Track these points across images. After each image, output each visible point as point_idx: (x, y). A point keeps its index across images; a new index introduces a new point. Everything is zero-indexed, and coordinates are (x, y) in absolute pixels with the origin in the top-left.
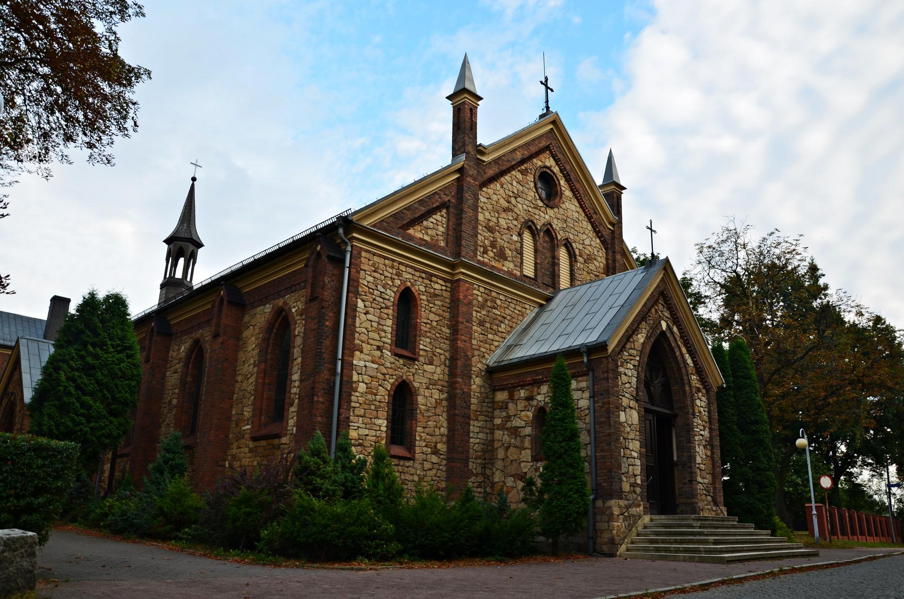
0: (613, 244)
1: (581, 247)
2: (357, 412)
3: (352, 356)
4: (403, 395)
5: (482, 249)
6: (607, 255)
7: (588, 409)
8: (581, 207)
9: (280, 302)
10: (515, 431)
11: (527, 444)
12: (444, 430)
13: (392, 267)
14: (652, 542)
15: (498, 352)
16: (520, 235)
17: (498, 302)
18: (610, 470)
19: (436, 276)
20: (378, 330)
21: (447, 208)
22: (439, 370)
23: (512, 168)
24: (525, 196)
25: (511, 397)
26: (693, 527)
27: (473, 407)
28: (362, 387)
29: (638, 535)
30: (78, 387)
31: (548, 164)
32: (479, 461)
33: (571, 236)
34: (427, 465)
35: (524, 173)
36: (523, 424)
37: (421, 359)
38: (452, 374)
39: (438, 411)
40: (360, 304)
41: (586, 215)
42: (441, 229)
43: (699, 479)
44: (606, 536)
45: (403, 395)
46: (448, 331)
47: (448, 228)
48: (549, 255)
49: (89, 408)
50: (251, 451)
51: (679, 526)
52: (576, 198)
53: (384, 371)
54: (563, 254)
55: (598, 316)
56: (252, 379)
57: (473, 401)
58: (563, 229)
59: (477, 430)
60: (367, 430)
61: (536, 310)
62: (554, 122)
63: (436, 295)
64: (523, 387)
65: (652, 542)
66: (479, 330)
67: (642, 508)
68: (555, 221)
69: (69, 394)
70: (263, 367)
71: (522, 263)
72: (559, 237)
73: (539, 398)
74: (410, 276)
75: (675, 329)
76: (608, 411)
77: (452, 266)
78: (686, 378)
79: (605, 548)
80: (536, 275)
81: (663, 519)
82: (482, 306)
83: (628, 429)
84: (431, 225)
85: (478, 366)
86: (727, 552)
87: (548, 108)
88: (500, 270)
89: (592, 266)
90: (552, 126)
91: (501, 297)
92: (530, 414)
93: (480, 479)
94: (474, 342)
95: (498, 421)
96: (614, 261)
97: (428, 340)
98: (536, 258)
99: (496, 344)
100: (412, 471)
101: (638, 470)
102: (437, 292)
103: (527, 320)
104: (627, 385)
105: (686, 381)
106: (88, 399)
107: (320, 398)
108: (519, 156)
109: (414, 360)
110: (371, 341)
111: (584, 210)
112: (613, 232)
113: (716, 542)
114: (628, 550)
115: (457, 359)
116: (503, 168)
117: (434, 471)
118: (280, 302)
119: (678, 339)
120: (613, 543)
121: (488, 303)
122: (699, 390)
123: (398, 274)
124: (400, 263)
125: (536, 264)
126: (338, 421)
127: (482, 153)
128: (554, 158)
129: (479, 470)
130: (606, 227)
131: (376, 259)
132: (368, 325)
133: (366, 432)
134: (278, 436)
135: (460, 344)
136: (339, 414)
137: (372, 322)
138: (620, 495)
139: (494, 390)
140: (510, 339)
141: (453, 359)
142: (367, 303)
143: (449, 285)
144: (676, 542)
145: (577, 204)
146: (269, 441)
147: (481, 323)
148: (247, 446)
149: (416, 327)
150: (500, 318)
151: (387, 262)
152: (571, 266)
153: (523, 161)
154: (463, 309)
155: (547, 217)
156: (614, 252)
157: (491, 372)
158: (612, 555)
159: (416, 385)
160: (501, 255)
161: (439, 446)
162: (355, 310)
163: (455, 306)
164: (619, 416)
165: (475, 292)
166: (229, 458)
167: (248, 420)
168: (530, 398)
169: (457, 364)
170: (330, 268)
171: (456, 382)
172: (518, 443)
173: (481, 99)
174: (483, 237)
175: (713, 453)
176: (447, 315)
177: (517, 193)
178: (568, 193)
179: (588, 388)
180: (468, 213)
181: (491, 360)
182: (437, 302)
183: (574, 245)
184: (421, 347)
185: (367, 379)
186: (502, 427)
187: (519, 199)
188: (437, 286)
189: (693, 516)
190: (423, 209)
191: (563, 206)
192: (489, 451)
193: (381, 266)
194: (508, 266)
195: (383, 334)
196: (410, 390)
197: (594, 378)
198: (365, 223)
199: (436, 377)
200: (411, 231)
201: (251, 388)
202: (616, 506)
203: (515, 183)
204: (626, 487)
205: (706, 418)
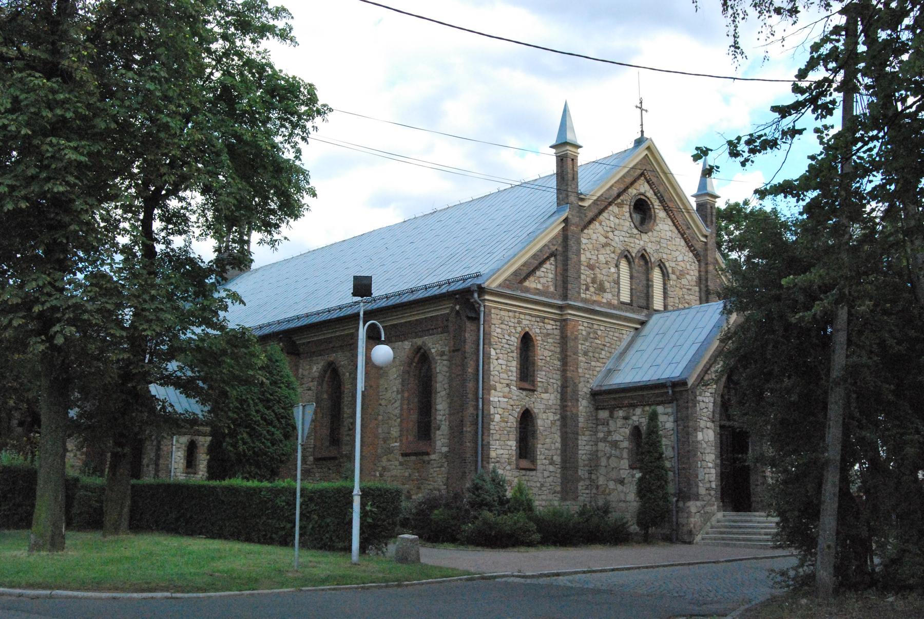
1: (673, 264)
2: (494, 438)
3: (489, 394)
4: (526, 418)
5: (584, 287)
9: (419, 341)
10: (615, 445)
11: (625, 455)
12: (558, 445)
13: (515, 317)
14: (721, 533)
15: (600, 376)
16: (617, 266)
17: (599, 333)
19: (548, 318)
20: (506, 371)
21: (555, 256)
23: (610, 204)
24: (621, 228)
25: (611, 416)
27: (580, 425)
28: (497, 418)
29: (712, 528)
31: (642, 191)
32: (587, 468)
33: (665, 256)
34: (546, 474)
35: (620, 205)
36: (622, 438)
37: (539, 389)
38: (563, 398)
39: (553, 430)
40: (493, 352)
41: (679, 232)
44: (685, 529)
45: (526, 418)
46: (559, 363)
47: (556, 275)
48: (643, 278)
50: (401, 464)
52: (670, 217)
53: (512, 403)
54: (656, 275)
55: (682, 352)
56: (397, 404)
57: (581, 419)
58: (657, 251)
59: (584, 443)
60: (502, 448)
61: (632, 334)
62: (648, 148)
63: (548, 335)
64: (621, 408)
65: (721, 533)
66: (584, 359)
67: (715, 507)
68: (649, 245)
70: (406, 395)
71: (619, 292)
72: (653, 260)
73: (635, 418)
74: (528, 322)
76: (688, 434)
77: (560, 308)
79: (686, 537)
81: (732, 515)
82: (586, 340)
83: (705, 445)
84: (542, 274)
85: (584, 390)
87: (642, 132)
88: (599, 303)
89: (684, 281)
90: (646, 152)
91: (602, 328)
92: (627, 431)
93: (588, 483)
94: (580, 370)
95: (601, 435)
96: (707, 272)
97: (544, 373)
98: (631, 284)
99: (598, 369)
100: (536, 479)
101: (713, 477)
102: (549, 332)
103: (624, 344)
104: (705, 410)
107: (468, 428)
108: (615, 191)
109: (534, 391)
110: (502, 381)
111: (677, 228)
112: (706, 243)
114: (703, 539)
115: (567, 387)
116: (604, 205)
117: (551, 479)
118: (419, 341)
120: (690, 533)
121: (592, 335)
124: (520, 313)
125: (631, 289)
126: (482, 445)
127: (582, 200)
128: (648, 182)
129: (587, 475)
130: (698, 240)
131: (502, 313)
132: (498, 368)
133: (502, 451)
134: (428, 454)
135: (569, 374)
136: (483, 440)
137: (502, 364)
138: (697, 497)
139: (597, 409)
140: (610, 364)
141: (564, 387)
142: (498, 351)
143: (558, 323)
146: (421, 457)
147: (585, 354)
148: (397, 460)
150: (601, 347)
151: (511, 314)
152: (665, 284)
153: (619, 195)
154: (571, 344)
155: (642, 243)
157: (595, 395)
158: (690, 543)
159: (536, 411)
160: (601, 289)
161: (555, 458)
162: (489, 358)
163: (565, 341)
164: (696, 437)
165: (580, 327)
166: (380, 469)
168: (626, 418)
169: (567, 391)
170: (469, 326)
171: (566, 406)
172: (618, 453)
173: (579, 147)
174: (586, 275)
176: (558, 350)
177: (617, 225)
178: (661, 214)
180: (571, 255)
181: (594, 384)
182: (550, 340)
183: (667, 264)
184: (539, 379)
186: (604, 440)
187: (616, 233)
188: (549, 327)
190: (536, 263)
191: (657, 228)
192: (594, 464)
193: (507, 318)
194: (607, 297)
195: (510, 374)
196: (531, 415)
197: (678, 406)
198: (494, 286)
199: (551, 402)
200: (527, 284)
201: (397, 412)
202: (693, 506)
203: (612, 218)
204: (702, 491)
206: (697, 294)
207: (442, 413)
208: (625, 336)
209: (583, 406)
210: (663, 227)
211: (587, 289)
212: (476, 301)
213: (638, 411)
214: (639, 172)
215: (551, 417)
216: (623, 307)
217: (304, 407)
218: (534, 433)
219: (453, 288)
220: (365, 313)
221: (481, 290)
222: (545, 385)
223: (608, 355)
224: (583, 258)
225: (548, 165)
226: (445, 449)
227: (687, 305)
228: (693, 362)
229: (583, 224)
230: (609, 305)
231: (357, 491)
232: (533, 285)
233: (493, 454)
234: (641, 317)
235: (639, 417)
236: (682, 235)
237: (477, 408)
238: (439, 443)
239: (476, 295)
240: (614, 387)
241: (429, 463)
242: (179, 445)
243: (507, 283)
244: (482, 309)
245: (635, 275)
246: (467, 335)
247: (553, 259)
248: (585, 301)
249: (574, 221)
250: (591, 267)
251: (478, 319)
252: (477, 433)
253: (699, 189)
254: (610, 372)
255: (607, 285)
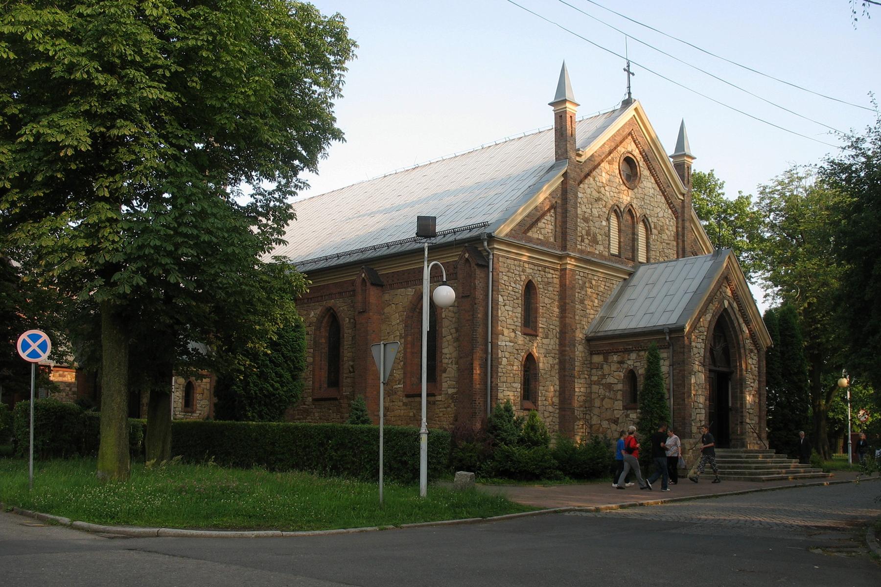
0: (683, 212)
1: (655, 220)
2: (502, 380)
4: (530, 362)
5: (580, 239)
6: (677, 223)
7: (668, 373)
8: (657, 183)
10: (609, 386)
16: (608, 220)
17: (594, 282)
18: (684, 419)
19: (548, 267)
22: (552, 342)
25: (606, 360)
26: (741, 457)
28: (504, 361)
30: (271, 361)
34: (546, 414)
36: (616, 381)
37: (540, 335)
39: (553, 373)
40: (501, 299)
42: (551, 227)
43: (748, 421)
45: (530, 362)
47: (556, 226)
49: (281, 376)
51: (732, 457)
52: (653, 175)
53: (518, 347)
57: (577, 364)
60: (509, 392)
61: (621, 284)
63: (549, 283)
69: (267, 366)
71: (609, 245)
73: (629, 362)
74: (531, 271)
75: (735, 305)
76: (683, 376)
77: (560, 258)
78: (741, 343)
80: (619, 252)
84: (543, 225)
85: (579, 335)
86: (763, 474)
87: (629, 93)
94: (577, 317)
96: (683, 228)
99: (592, 316)
101: (703, 417)
102: (550, 280)
105: (742, 346)
106: (279, 369)
108: (607, 149)
109: (537, 336)
111: (659, 186)
113: (756, 468)
119: (737, 312)
122: (751, 351)
123: (524, 271)
125: (620, 242)
128: (634, 141)
131: (509, 261)
137: (509, 313)
139: (591, 354)
143: (558, 273)
144: (729, 468)
145: (653, 181)
149: (536, 309)
152: (647, 238)
153: (610, 153)
156: (683, 220)
165: (577, 277)
167: (400, 381)
168: (621, 362)
170: (479, 273)
171: (565, 351)
174: (582, 226)
175: (760, 400)
178: (646, 172)
179: (668, 358)
183: (650, 219)
185: (507, 354)
186: (598, 383)
188: (550, 276)
189: (742, 450)
191: (642, 185)
197: (674, 351)
198: (502, 235)
200: (530, 234)
204: (694, 430)
205: (756, 373)
206: (675, 249)
207: (448, 356)
208: (615, 286)
209: (580, 351)
210: (648, 184)
211: (582, 241)
212: (485, 250)
213: (633, 356)
214: (627, 131)
215: (551, 361)
216: (613, 258)
217: (385, 345)
218: (536, 375)
219: (459, 237)
220: (430, 248)
221: (491, 238)
222: (546, 330)
223: (601, 303)
224: (579, 211)
225: (550, 121)
226: (450, 391)
227: (666, 259)
228: (687, 311)
229: (579, 179)
230: (601, 255)
231: (32, 406)
232: (535, 236)
233: (500, 395)
234: (629, 267)
235: (636, 362)
236: (663, 193)
237: (486, 351)
238: (445, 385)
239: (486, 244)
240: (609, 333)
241: (434, 404)
242: (177, 386)
243: (513, 233)
244: (491, 257)
245: (623, 228)
246: (477, 282)
247: (552, 211)
248: (581, 252)
249: (572, 176)
250: (586, 220)
251: (488, 267)
252: (486, 375)
253: (677, 150)
254: (603, 319)
255: (599, 237)
